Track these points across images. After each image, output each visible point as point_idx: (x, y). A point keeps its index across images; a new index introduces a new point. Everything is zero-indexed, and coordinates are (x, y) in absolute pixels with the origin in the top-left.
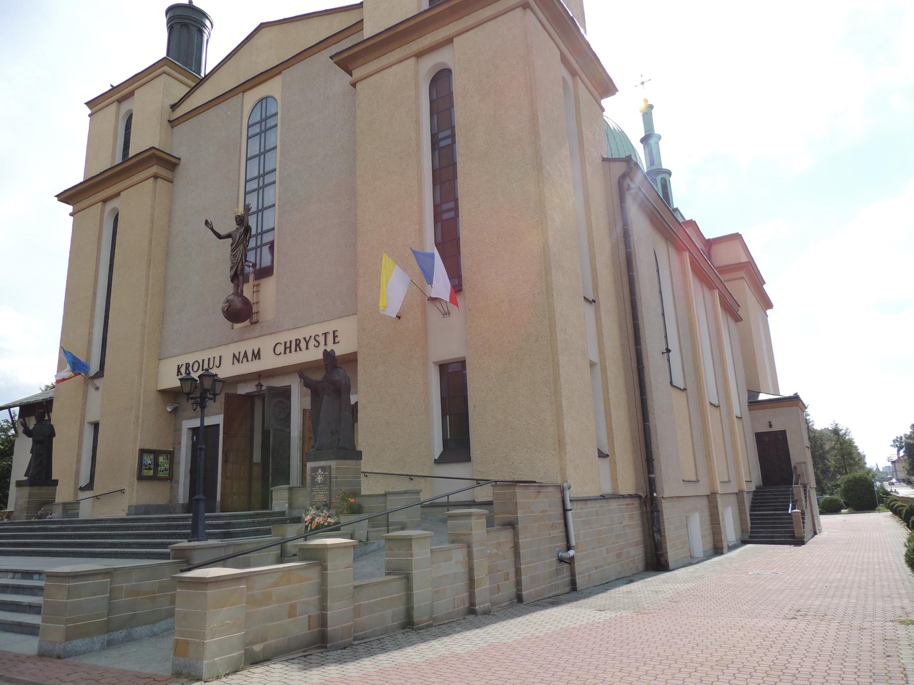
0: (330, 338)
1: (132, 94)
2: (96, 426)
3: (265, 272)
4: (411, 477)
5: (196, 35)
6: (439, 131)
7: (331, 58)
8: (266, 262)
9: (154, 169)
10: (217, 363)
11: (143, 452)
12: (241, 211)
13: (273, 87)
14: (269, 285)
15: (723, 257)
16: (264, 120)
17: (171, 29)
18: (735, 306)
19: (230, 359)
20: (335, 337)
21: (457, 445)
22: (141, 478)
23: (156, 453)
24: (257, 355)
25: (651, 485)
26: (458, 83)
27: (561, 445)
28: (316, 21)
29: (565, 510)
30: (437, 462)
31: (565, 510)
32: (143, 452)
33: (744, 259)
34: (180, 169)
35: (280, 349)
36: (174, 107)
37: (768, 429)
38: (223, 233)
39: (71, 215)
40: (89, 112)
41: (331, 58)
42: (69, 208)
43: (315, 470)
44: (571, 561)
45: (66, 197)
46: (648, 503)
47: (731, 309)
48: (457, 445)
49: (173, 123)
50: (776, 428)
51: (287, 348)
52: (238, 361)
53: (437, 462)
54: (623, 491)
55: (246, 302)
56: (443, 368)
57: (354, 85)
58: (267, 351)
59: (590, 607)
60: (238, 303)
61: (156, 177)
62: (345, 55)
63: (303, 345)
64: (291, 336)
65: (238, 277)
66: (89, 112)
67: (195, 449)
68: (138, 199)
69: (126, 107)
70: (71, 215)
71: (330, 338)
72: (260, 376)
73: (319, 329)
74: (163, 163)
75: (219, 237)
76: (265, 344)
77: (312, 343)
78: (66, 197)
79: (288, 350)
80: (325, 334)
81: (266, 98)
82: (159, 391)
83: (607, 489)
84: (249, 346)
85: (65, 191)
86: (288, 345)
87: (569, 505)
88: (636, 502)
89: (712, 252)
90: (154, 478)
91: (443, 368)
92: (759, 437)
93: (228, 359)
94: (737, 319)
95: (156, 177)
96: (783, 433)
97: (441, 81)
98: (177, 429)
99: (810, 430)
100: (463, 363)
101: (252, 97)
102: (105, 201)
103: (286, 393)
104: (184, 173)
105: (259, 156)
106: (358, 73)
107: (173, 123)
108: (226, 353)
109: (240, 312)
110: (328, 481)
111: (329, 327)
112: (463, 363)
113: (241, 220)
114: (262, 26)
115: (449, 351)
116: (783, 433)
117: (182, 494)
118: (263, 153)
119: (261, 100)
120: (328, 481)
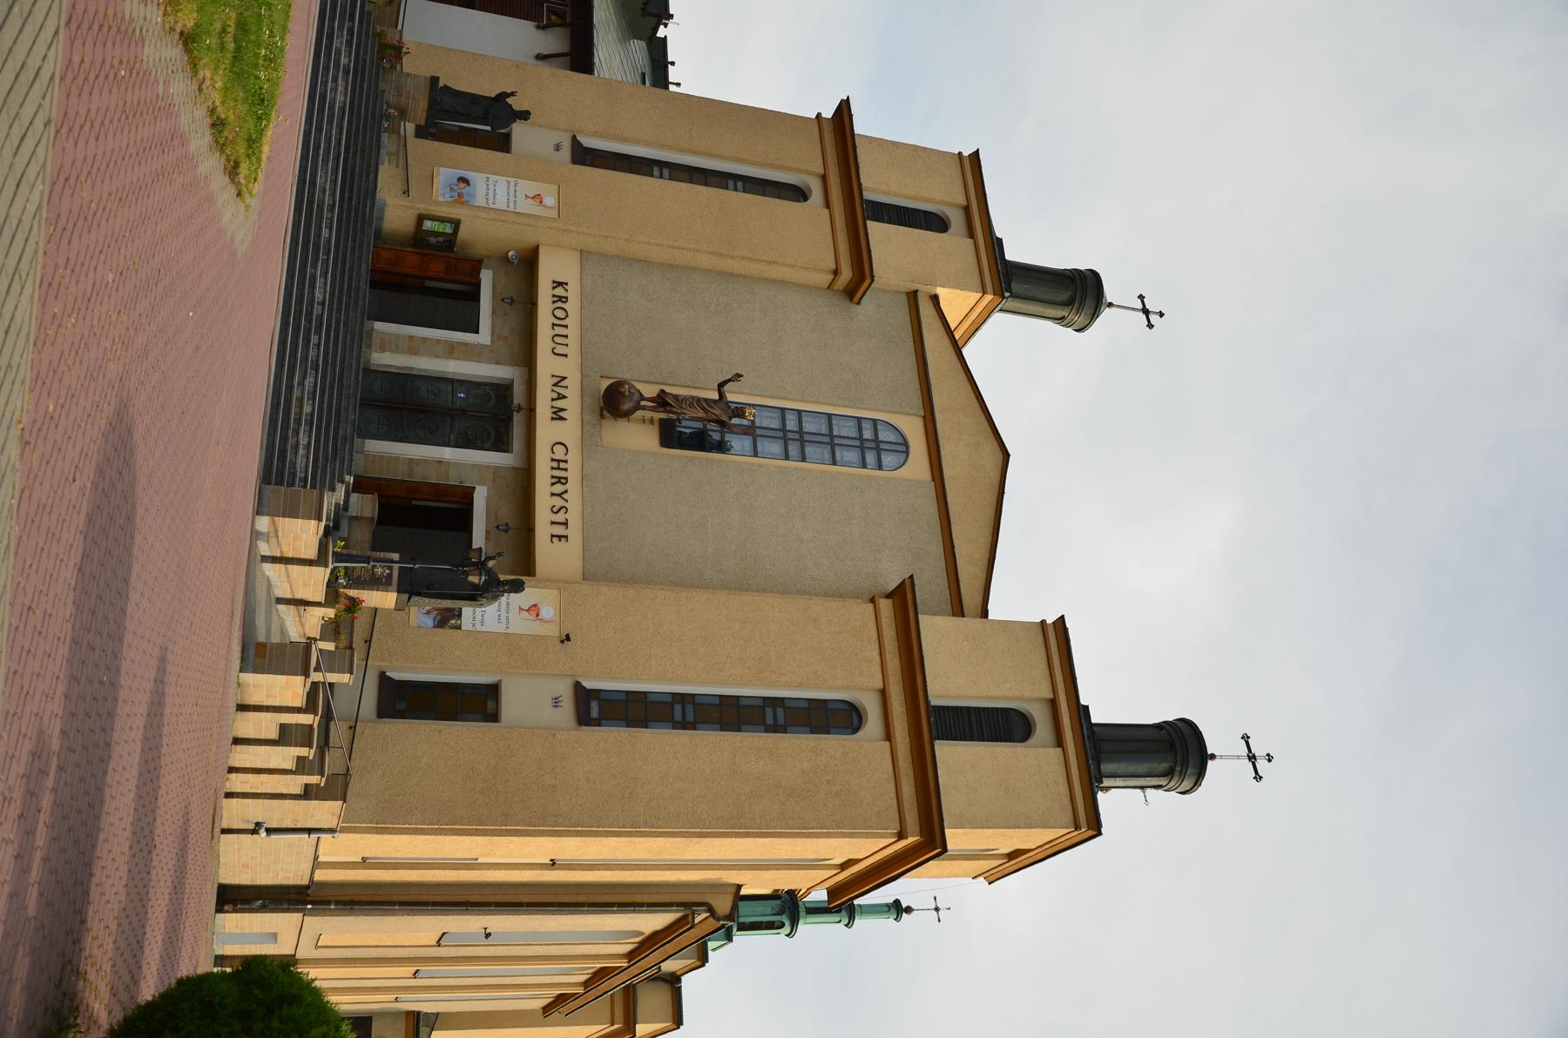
0: (560, 530)
4: (368, 642)
6: (785, 708)
7: (911, 577)
9: (847, 274)
10: (559, 350)
13: (917, 466)
18: (565, 1009)
19: (559, 366)
20: (560, 537)
24: (558, 415)
26: (833, 743)
28: (985, 540)
29: (309, 831)
30: (382, 675)
31: (309, 831)
35: (559, 453)
39: (819, 115)
40: (966, 154)
41: (911, 577)
42: (828, 113)
43: (390, 568)
45: (844, 109)
46: (300, 897)
49: (913, 296)
51: (558, 464)
52: (555, 385)
56: (493, 690)
58: (557, 433)
62: (909, 596)
63: (558, 488)
64: (573, 472)
65: (662, 401)
66: (966, 154)
70: (819, 115)
71: (560, 530)
72: (531, 410)
73: (574, 516)
74: (857, 278)
75: (721, 385)
76: (569, 431)
77: (558, 502)
78: (844, 109)
79: (555, 464)
80: (566, 524)
81: (907, 452)
82: (535, 252)
84: (572, 405)
85: (851, 116)
86: (562, 465)
87: (314, 836)
89: (661, 984)
91: (493, 690)
94: (547, 1010)
95: (836, 272)
99: (378, 233)
100: (494, 717)
101: (913, 429)
102: (824, 178)
103: (501, 445)
105: (831, 435)
106: (886, 606)
108: (570, 367)
109: (614, 402)
111: (574, 531)
112: (494, 717)
119: (906, 444)
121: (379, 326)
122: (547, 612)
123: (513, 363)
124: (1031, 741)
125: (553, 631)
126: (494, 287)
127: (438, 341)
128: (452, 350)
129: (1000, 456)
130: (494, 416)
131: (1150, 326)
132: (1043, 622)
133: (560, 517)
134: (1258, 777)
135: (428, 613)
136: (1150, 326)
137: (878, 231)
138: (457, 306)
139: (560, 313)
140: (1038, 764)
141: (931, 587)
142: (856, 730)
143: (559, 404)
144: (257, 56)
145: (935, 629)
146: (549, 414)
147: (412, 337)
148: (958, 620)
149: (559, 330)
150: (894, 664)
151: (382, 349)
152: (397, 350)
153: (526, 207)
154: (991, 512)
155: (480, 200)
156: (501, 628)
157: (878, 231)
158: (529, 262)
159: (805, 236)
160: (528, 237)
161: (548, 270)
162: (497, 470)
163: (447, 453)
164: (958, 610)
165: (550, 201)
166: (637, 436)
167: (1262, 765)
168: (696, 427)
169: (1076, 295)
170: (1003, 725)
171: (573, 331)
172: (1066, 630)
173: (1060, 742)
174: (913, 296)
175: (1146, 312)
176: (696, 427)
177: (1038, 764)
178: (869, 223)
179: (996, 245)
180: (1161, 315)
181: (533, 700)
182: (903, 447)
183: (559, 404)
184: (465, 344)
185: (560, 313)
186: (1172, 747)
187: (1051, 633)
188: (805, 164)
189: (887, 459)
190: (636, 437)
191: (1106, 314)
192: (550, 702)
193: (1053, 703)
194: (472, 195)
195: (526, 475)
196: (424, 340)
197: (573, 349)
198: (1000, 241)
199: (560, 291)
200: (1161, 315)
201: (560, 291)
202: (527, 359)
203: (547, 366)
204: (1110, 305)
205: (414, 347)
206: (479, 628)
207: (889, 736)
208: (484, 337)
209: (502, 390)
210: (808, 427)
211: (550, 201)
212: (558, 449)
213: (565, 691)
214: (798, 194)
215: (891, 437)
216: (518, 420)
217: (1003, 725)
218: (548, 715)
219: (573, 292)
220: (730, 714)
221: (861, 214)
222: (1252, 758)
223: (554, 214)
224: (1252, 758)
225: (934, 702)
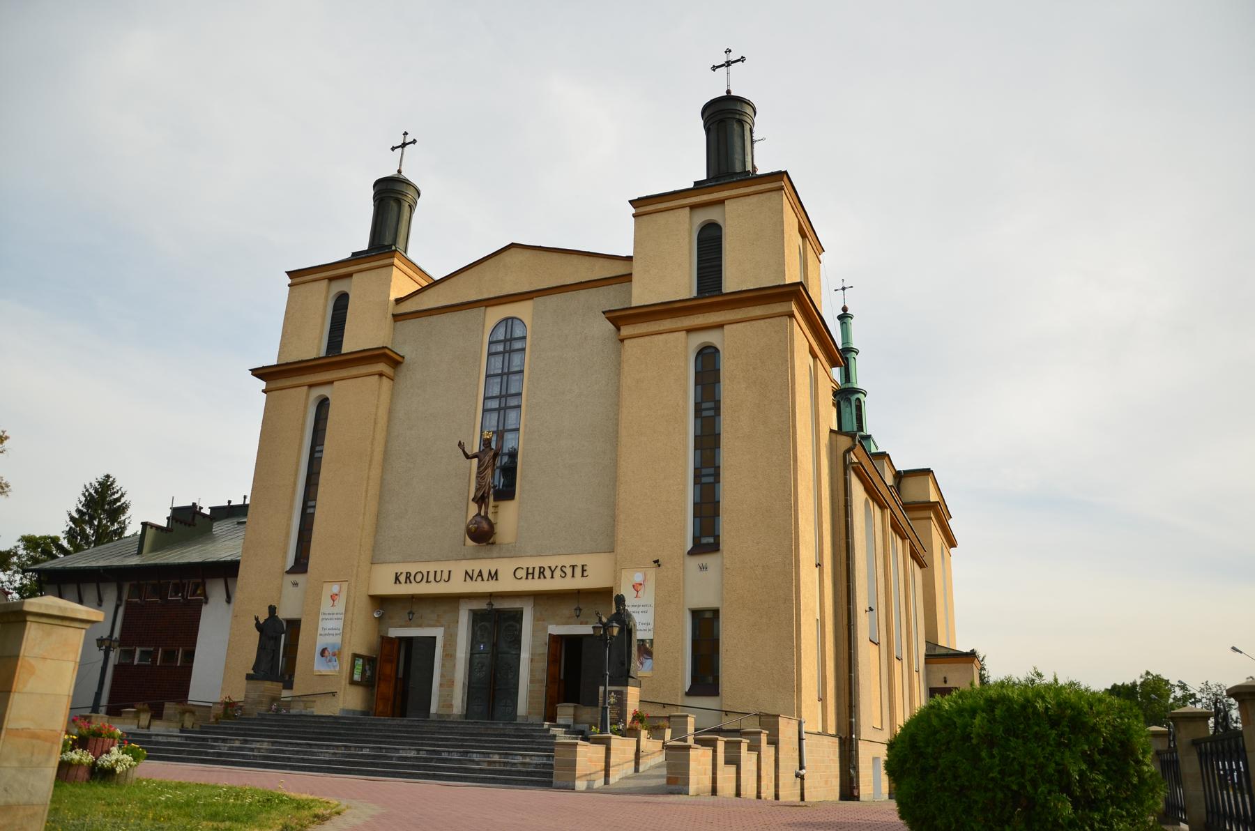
0: (578, 571)
1: (350, 275)
4: (664, 705)
5: (736, 127)
6: (702, 401)
9: (382, 367)
10: (445, 576)
13: (522, 310)
15: (912, 491)
16: (509, 340)
19: (458, 576)
20: (583, 571)
24: (494, 576)
26: (727, 366)
29: (800, 739)
30: (688, 694)
31: (800, 739)
33: (934, 498)
34: (403, 367)
39: (264, 391)
40: (289, 281)
42: (262, 384)
44: (802, 778)
45: (259, 373)
47: (919, 557)
51: (529, 574)
53: (688, 694)
56: (696, 614)
57: (622, 340)
58: (507, 576)
59: (962, 695)
62: (618, 314)
63: (548, 573)
64: (536, 563)
65: (481, 500)
66: (289, 281)
70: (264, 391)
71: (578, 571)
72: (491, 596)
73: (567, 561)
75: (467, 457)
76: (505, 567)
77: (558, 573)
78: (259, 373)
81: (513, 318)
84: (486, 566)
87: (804, 736)
89: (902, 485)
91: (696, 614)
93: (458, 576)
95: (381, 375)
100: (716, 612)
101: (495, 315)
103: (517, 616)
105: (501, 375)
106: (626, 331)
108: (458, 569)
109: (482, 535)
111: (579, 561)
112: (716, 612)
114: (513, 245)
115: (705, 600)
118: (507, 374)
121: (433, 709)
122: (638, 577)
123: (457, 610)
124: (720, 222)
125: (652, 572)
126: (401, 626)
127: (443, 665)
128: (449, 656)
129: (513, 250)
131: (414, 142)
132: (634, 216)
133: (569, 571)
134: (742, 59)
135: (642, 664)
137: (348, 346)
139: (419, 578)
140: (738, 218)
141: (610, 298)
142: (717, 350)
143: (485, 575)
145: (642, 294)
146: (493, 582)
147: (441, 685)
149: (431, 578)
150: (667, 324)
151: (451, 706)
152: (450, 695)
153: (340, 606)
154: (555, 255)
155: (338, 640)
156: (651, 610)
158: (382, 603)
159: (354, 397)
162: (536, 619)
163: (525, 655)
164: (627, 278)
165: (335, 588)
166: (507, 517)
167: (733, 57)
168: (499, 475)
169: (392, 197)
170: (710, 244)
171: (431, 567)
172: (639, 199)
173: (721, 202)
174: (397, 317)
175: (404, 145)
176: (499, 475)
177: (738, 218)
179: (357, 257)
180: (406, 134)
181: (703, 585)
182: (509, 321)
183: (485, 575)
184: (444, 646)
185: (419, 578)
186: (722, 121)
188: (302, 401)
189: (518, 333)
190: (507, 517)
191: (406, 174)
192: (704, 573)
194: (334, 645)
195: (539, 597)
196: (442, 676)
197: (444, 567)
198: (696, 183)
199: (402, 578)
200: (406, 134)
201: (402, 578)
202: (453, 600)
203: (458, 586)
204: (399, 171)
205: (448, 683)
206: (651, 626)
207: (720, 326)
208: (438, 633)
209: (476, 617)
210: (496, 392)
211: (335, 588)
212: (519, 574)
215: (502, 330)
216: (499, 605)
217: (710, 244)
218: (713, 574)
219: (403, 568)
220: (708, 441)
222: (728, 64)
223: (345, 585)
224: (728, 64)
225: (695, 294)
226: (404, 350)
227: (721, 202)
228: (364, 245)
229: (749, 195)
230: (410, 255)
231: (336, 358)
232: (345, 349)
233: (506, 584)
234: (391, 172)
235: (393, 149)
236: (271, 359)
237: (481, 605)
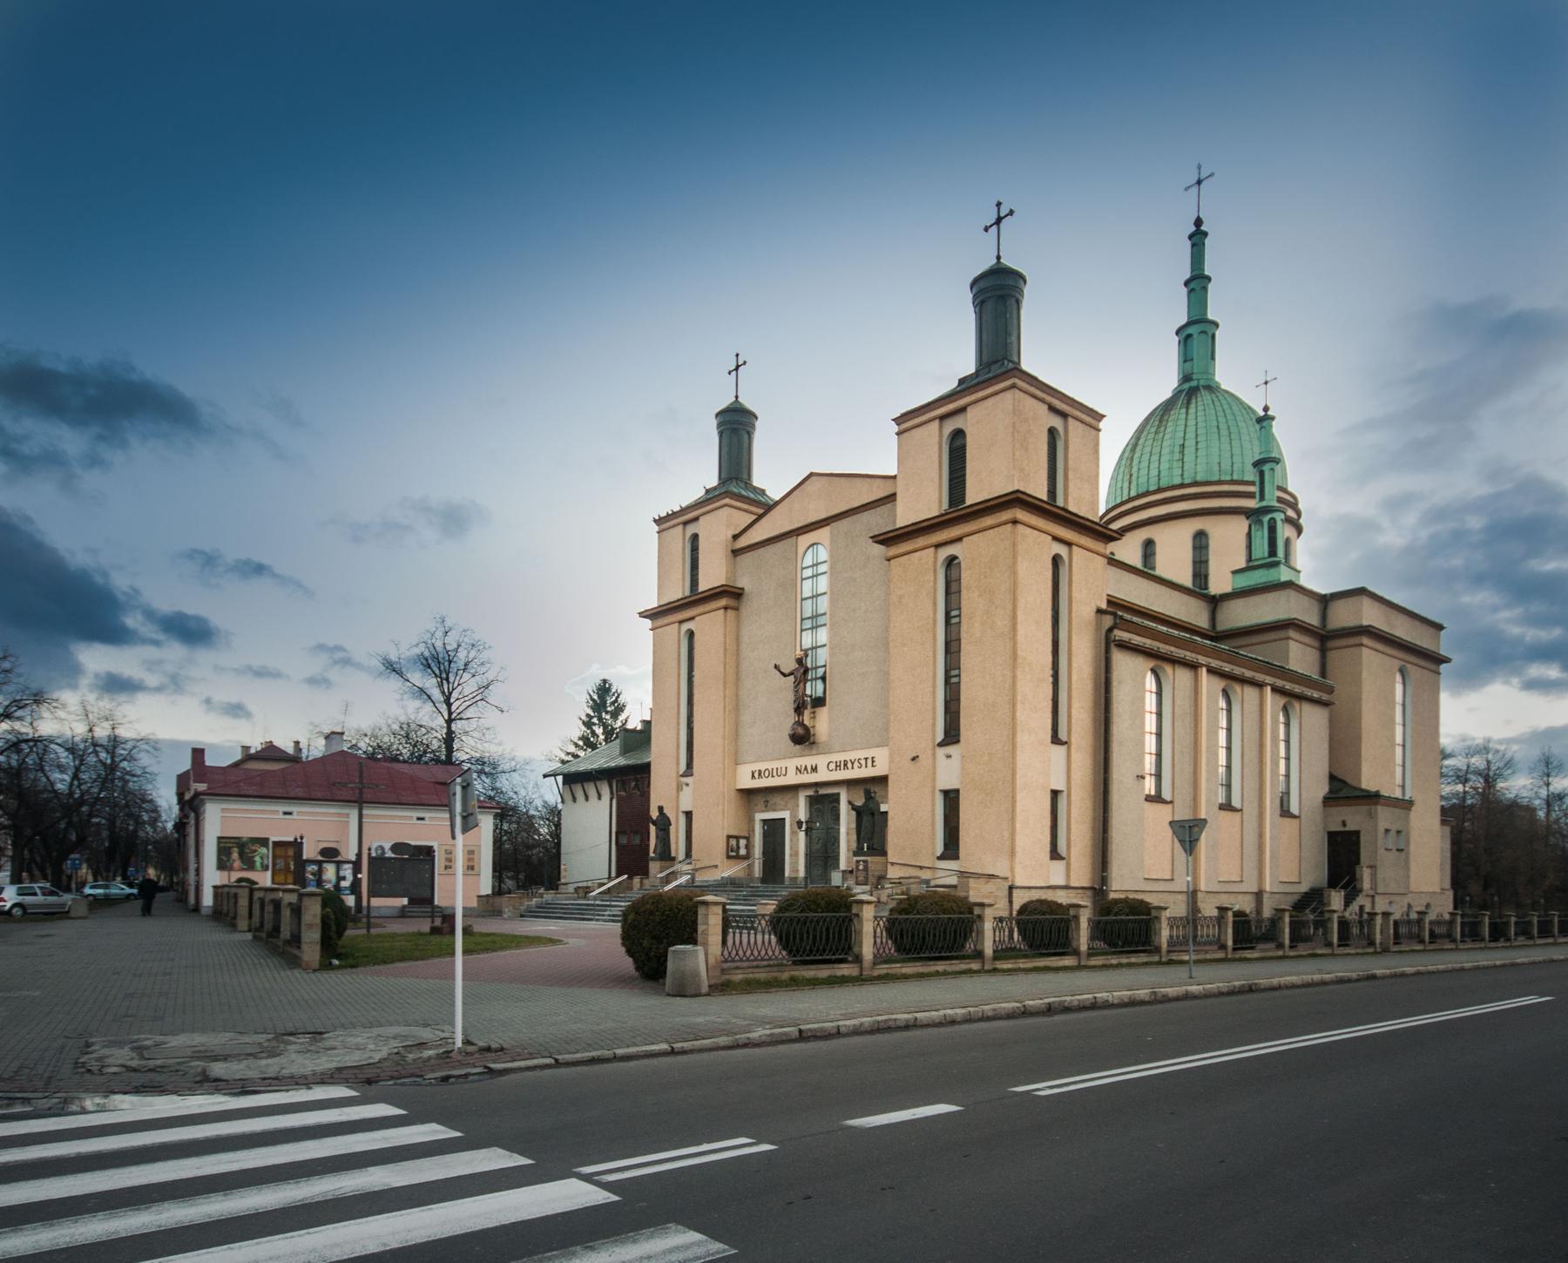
2: (689, 814)
3: (819, 702)
4: (921, 868)
8: (820, 693)
9: (723, 602)
11: (729, 837)
12: (799, 653)
14: (823, 713)
17: (721, 434)
19: (791, 768)
21: (951, 848)
22: (729, 857)
23: (737, 838)
24: (814, 769)
25: (1104, 880)
26: (966, 576)
27: (1013, 853)
32: (729, 837)
34: (744, 599)
35: (832, 766)
36: (735, 537)
37: (1341, 829)
38: (786, 671)
45: (643, 615)
48: (951, 848)
50: (1350, 827)
51: (838, 766)
54: (1074, 884)
55: (806, 729)
56: (946, 793)
58: (823, 768)
60: (800, 731)
61: (726, 608)
64: (841, 757)
65: (799, 709)
66: (656, 528)
67: (766, 835)
68: (710, 625)
69: (691, 529)
72: (817, 785)
74: (731, 595)
75: (784, 675)
76: (821, 761)
78: (643, 615)
83: (1062, 882)
84: (808, 761)
88: (1089, 893)
90: (738, 857)
92: (1332, 836)
96: (1357, 833)
97: (951, 561)
98: (751, 820)
102: (681, 622)
103: (835, 799)
104: (749, 607)
107: (736, 553)
109: (802, 738)
110: (866, 869)
111: (869, 753)
112: (957, 791)
113: (800, 661)
114: (811, 475)
115: (947, 780)
116: (1357, 833)
117: (757, 871)
120: (866, 869)
121: (787, 874)
130: (823, 801)
131: (1011, 213)
136: (1011, 213)
137: (973, 496)
138: (774, 830)
141: (878, 522)
144: (147, 851)
145: (906, 513)
148: (899, 497)
157: (973, 496)
158: (748, 794)
160: (733, 793)
161: (747, 783)
163: (843, 830)
164: (892, 497)
166: (822, 724)
169: (736, 426)
172: (903, 415)
174: (736, 553)
175: (999, 221)
178: (969, 502)
179: (967, 385)
181: (949, 770)
187: (904, 426)
190: (822, 724)
191: (747, 402)
193: (942, 418)
198: (961, 381)
200: (999, 204)
203: (792, 779)
204: (998, 258)
205: (795, 854)
207: (959, 539)
210: (808, 613)
213: (941, 752)
214: (691, 634)
216: (823, 791)
218: (955, 762)
219: (757, 767)
220: (952, 648)
221: (696, 599)
226: (743, 582)
227: (963, 410)
228: (968, 366)
229: (996, 393)
230: (1025, 366)
231: (696, 599)
232: (969, 502)
233: (823, 775)
234: (726, 401)
235: (986, 229)
236: (652, 603)
237: (810, 792)
